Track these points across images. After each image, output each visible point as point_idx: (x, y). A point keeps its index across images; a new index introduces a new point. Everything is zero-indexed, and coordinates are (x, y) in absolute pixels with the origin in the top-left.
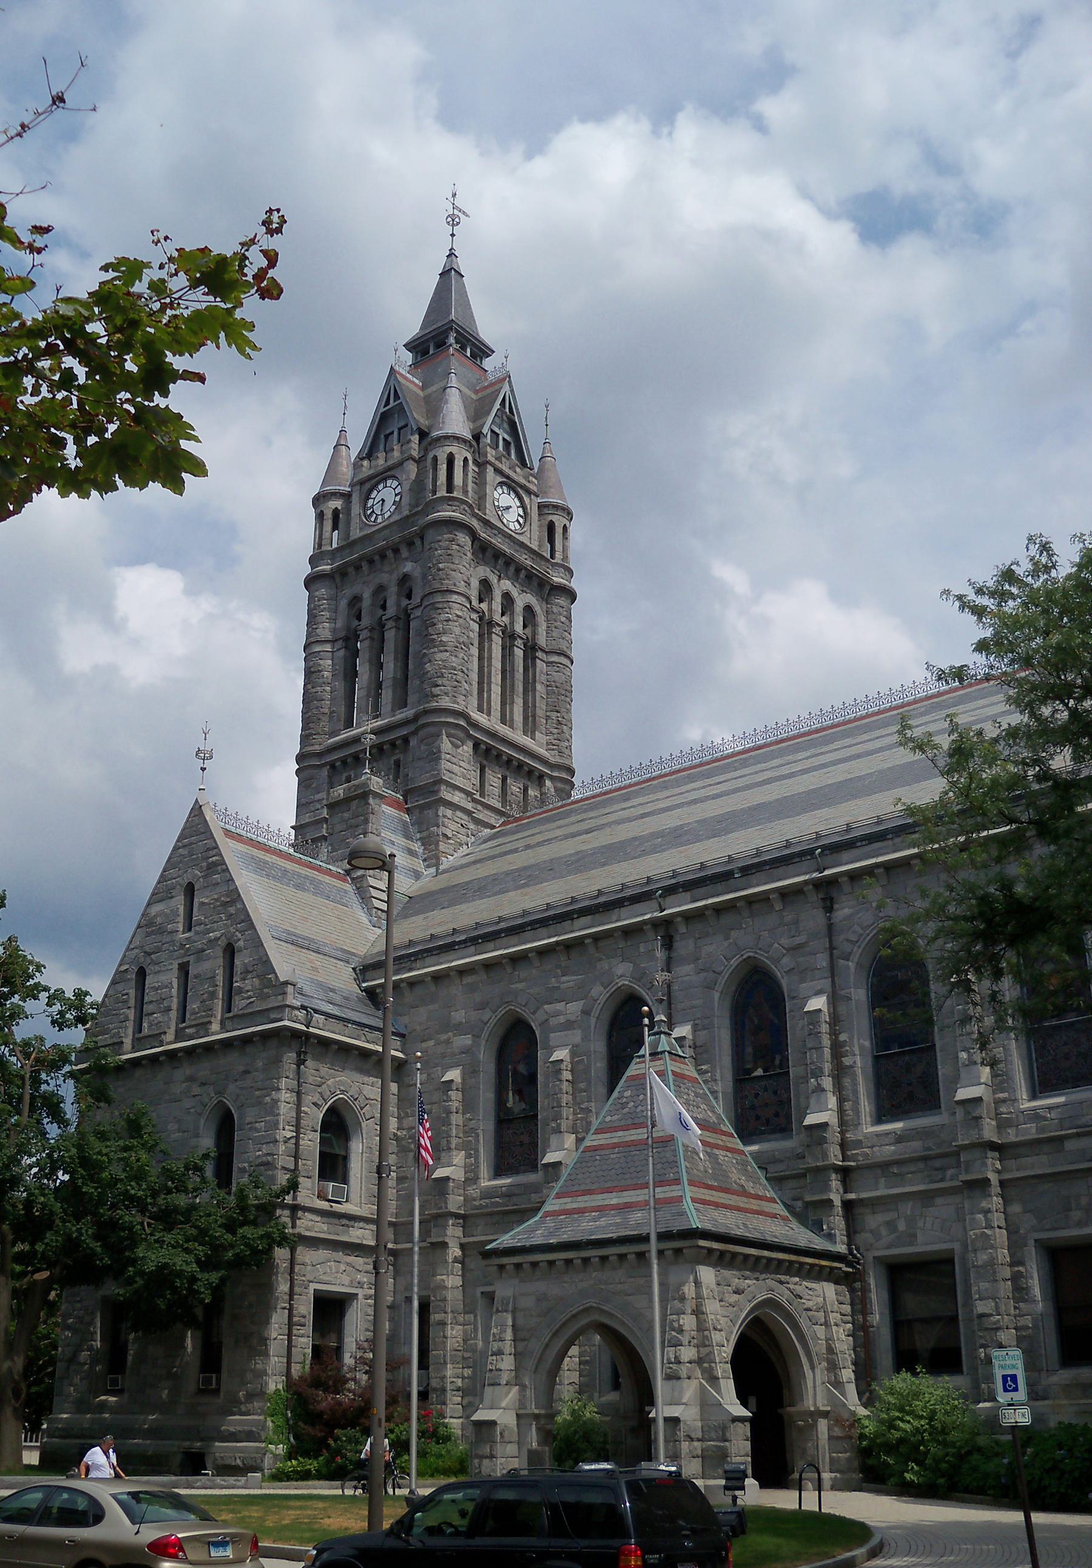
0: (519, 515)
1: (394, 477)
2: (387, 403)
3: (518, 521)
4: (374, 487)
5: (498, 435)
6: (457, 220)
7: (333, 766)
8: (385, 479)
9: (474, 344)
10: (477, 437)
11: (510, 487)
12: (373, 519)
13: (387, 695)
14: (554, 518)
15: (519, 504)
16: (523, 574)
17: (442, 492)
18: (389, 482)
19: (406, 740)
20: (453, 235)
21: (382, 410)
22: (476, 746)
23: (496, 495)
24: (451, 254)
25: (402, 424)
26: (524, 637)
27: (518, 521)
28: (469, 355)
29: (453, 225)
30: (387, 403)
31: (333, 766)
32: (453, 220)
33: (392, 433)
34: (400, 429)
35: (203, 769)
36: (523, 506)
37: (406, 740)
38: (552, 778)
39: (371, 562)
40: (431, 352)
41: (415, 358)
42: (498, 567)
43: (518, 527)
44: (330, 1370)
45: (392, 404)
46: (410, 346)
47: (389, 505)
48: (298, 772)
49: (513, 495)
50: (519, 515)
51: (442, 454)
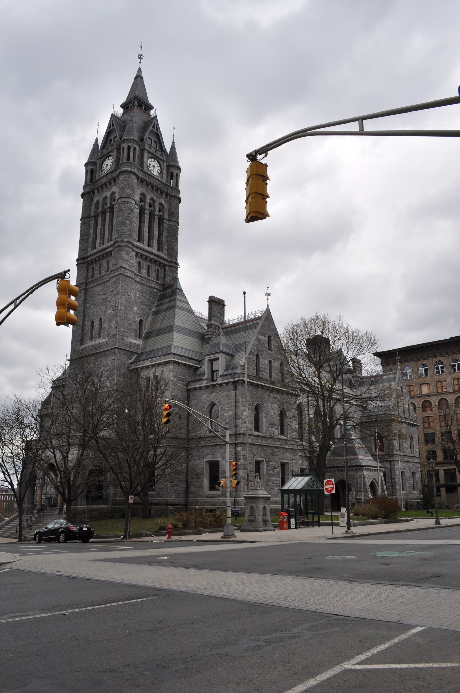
0: (158, 169)
1: (110, 156)
2: (110, 128)
3: (158, 172)
4: (104, 160)
5: (151, 139)
6: (142, 56)
7: (88, 263)
8: (108, 157)
9: (145, 105)
10: (142, 140)
11: (155, 159)
12: (104, 172)
13: (98, 241)
14: (173, 170)
15: (158, 165)
16: (159, 191)
17: (125, 160)
18: (110, 157)
19: (111, 252)
20: (140, 63)
21: (108, 131)
22: (137, 254)
23: (149, 162)
24: (139, 70)
25: (115, 136)
26: (159, 215)
27: (158, 172)
28: (143, 109)
29: (140, 59)
30: (110, 128)
31: (88, 263)
32: (141, 57)
33: (112, 139)
34: (114, 138)
35: (268, 299)
36: (160, 166)
37: (111, 252)
38: (168, 266)
39: (98, 190)
40: (129, 108)
41: (124, 111)
42: (149, 189)
43: (158, 174)
44: (57, 480)
45: (111, 128)
46: (122, 106)
47: (109, 167)
48: (77, 265)
49: (156, 162)
50: (158, 169)
51: (125, 146)
